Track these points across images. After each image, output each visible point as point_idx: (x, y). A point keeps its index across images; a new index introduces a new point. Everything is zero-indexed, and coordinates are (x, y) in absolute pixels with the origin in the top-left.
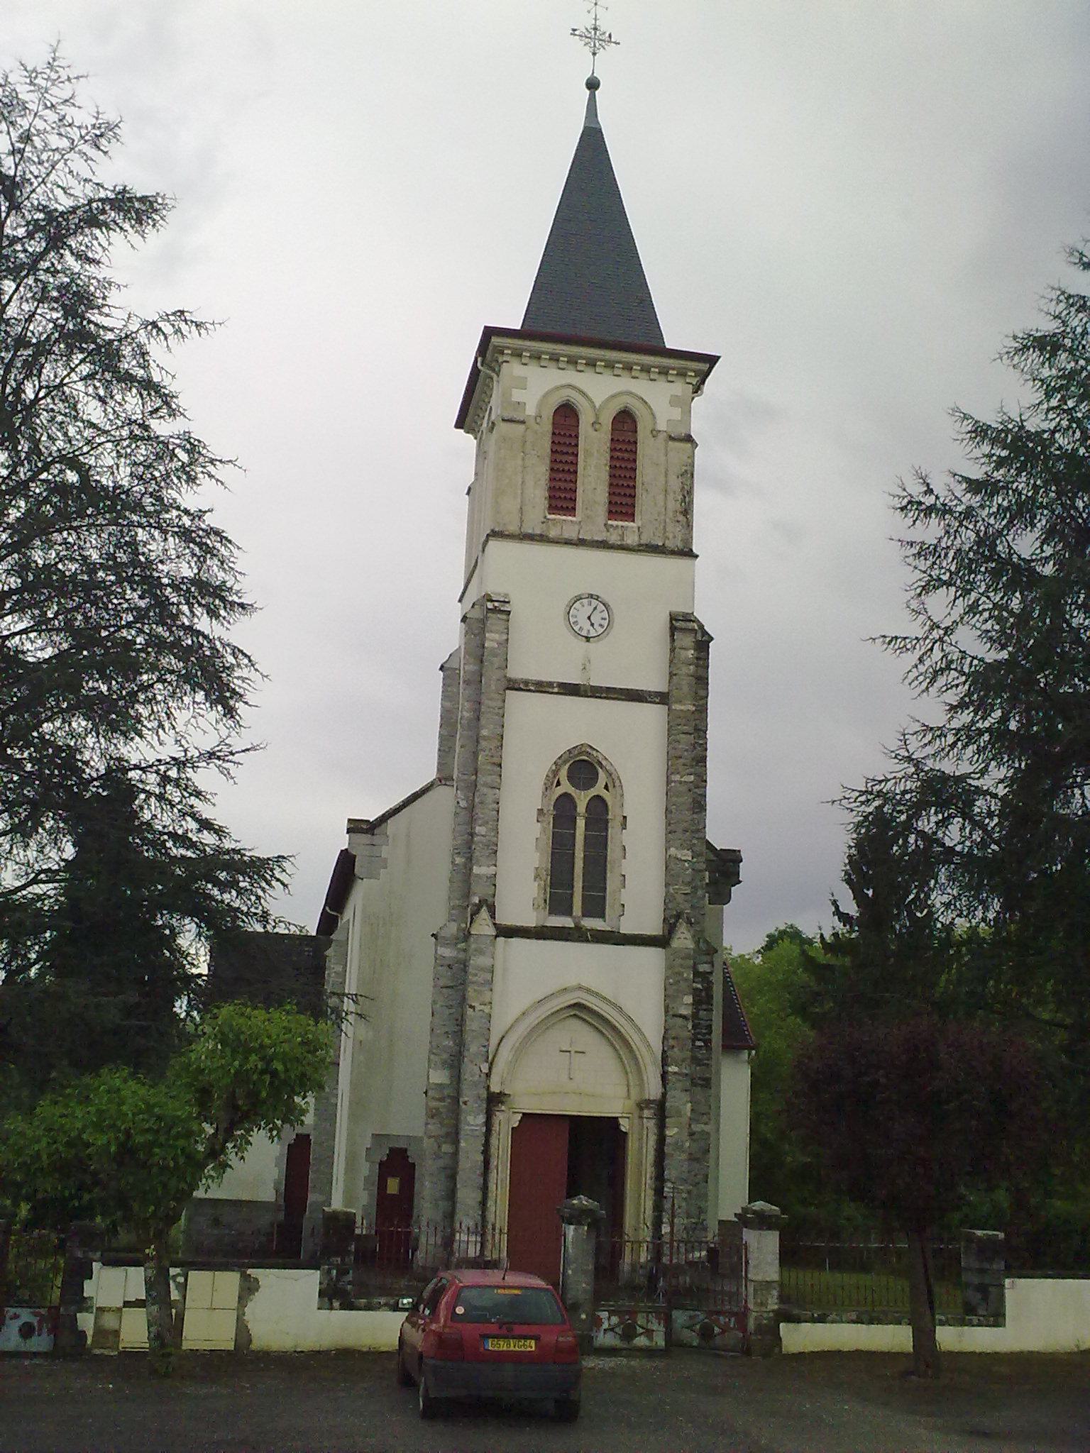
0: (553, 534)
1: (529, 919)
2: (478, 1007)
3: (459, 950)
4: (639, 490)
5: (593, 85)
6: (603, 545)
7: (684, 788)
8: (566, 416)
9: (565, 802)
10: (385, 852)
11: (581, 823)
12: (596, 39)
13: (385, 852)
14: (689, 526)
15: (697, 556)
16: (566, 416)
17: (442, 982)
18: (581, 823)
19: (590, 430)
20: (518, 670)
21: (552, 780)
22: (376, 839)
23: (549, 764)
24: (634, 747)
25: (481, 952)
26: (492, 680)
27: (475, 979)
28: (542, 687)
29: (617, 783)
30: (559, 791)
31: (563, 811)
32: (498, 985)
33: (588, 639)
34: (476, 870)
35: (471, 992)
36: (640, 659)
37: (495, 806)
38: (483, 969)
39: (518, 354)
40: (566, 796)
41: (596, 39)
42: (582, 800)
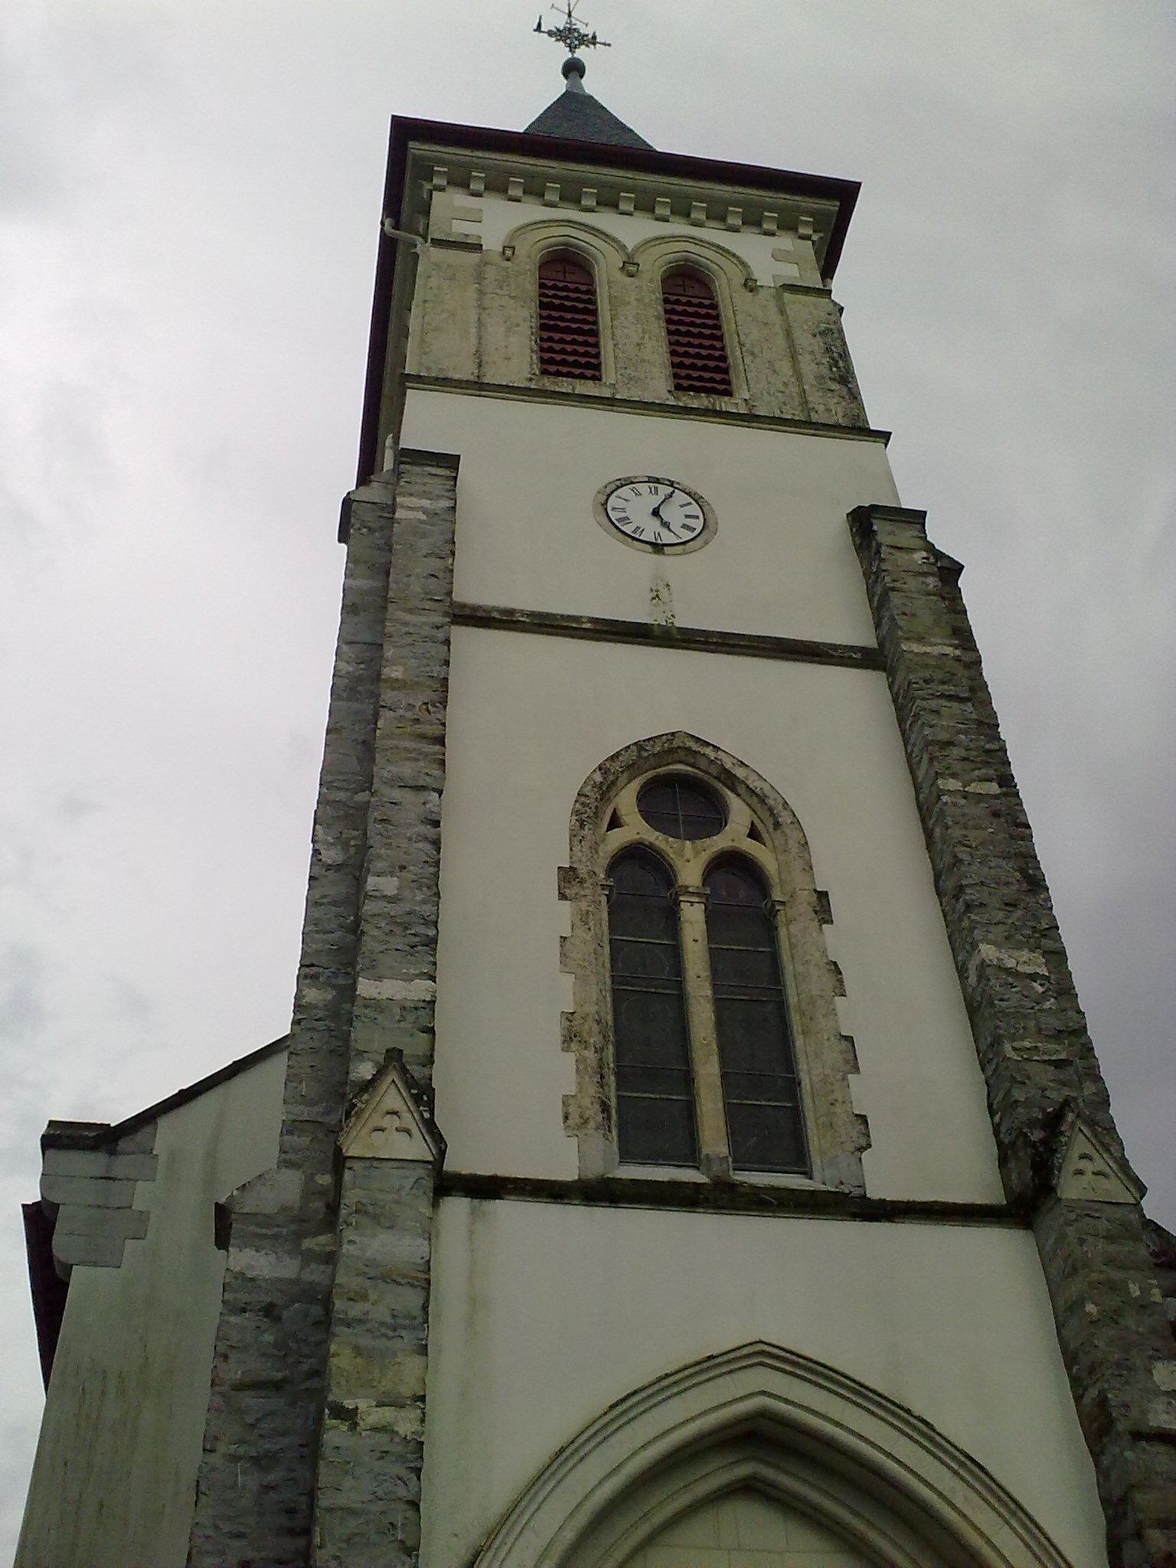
1: (564, 1163)
2: (372, 1415)
3: (308, 1257)
7: (979, 810)
10: (143, 1196)
11: (693, 916)
12: (569, 36)
13: (143, 1196)
14: (855, 396)
15: (885, 436)
17: (234, 1372)
18: (693, 916)
19: (620, 276)
21: (594, 807)
22: (122, 1165)
25: (376, 1216)
27: (356, 1310)
29: (785, 818)
30: (617, 839)
31: (635, 890)
32: (448, 1330)
33: (658, 548)
34: (365, 987)
35: (342, 1358)
36: (790, 573)
37: (429, 831)
38: (389, 1277)
40: (636, 855)
41: (569, 36)
42: (690, 863)
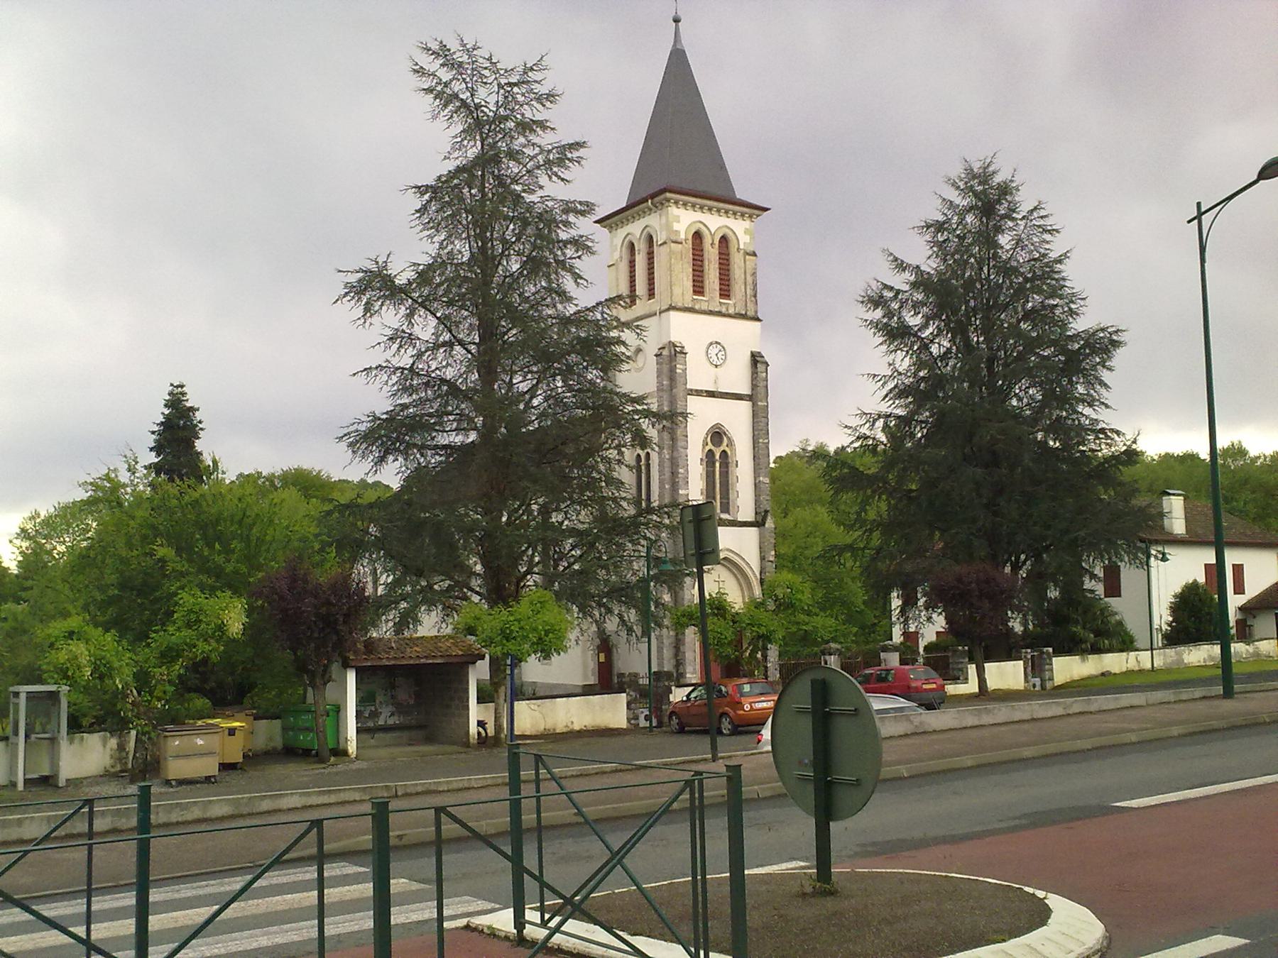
0: (697, 307)
4: (732, 282)
5: (677, 21)
6: (719, 314)
8: (698, 236)
9: (710, 454)
11: (718, 465)
16: (698, 236)
18: (718, 465)
20: (691, 385)
23: (704, 435)
24: (737, 419)
26: (679, 391)
28: (698, 393)
30: (707, 448)
39: (676, 203)
